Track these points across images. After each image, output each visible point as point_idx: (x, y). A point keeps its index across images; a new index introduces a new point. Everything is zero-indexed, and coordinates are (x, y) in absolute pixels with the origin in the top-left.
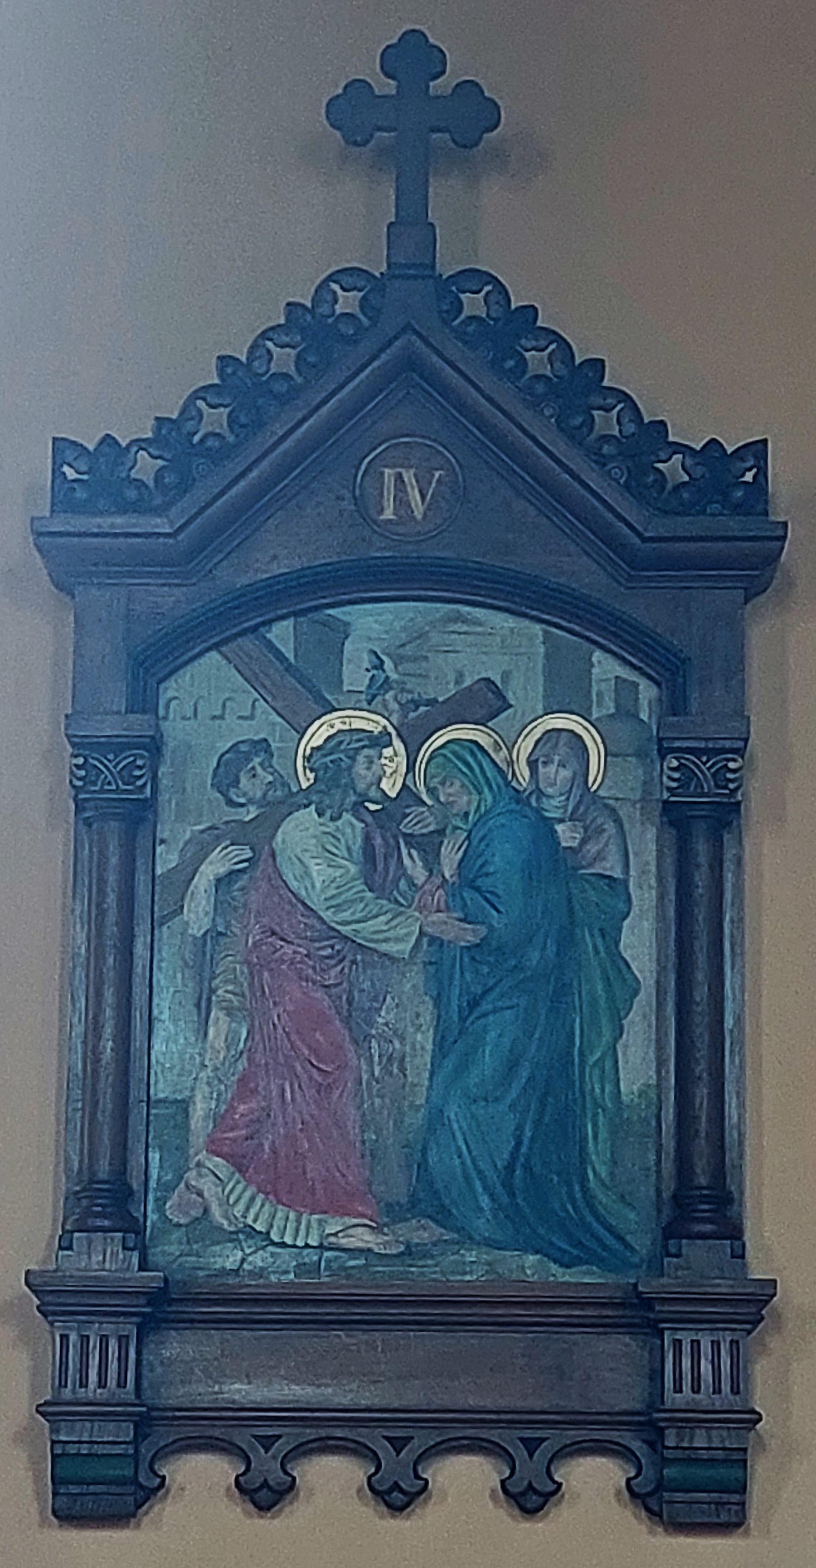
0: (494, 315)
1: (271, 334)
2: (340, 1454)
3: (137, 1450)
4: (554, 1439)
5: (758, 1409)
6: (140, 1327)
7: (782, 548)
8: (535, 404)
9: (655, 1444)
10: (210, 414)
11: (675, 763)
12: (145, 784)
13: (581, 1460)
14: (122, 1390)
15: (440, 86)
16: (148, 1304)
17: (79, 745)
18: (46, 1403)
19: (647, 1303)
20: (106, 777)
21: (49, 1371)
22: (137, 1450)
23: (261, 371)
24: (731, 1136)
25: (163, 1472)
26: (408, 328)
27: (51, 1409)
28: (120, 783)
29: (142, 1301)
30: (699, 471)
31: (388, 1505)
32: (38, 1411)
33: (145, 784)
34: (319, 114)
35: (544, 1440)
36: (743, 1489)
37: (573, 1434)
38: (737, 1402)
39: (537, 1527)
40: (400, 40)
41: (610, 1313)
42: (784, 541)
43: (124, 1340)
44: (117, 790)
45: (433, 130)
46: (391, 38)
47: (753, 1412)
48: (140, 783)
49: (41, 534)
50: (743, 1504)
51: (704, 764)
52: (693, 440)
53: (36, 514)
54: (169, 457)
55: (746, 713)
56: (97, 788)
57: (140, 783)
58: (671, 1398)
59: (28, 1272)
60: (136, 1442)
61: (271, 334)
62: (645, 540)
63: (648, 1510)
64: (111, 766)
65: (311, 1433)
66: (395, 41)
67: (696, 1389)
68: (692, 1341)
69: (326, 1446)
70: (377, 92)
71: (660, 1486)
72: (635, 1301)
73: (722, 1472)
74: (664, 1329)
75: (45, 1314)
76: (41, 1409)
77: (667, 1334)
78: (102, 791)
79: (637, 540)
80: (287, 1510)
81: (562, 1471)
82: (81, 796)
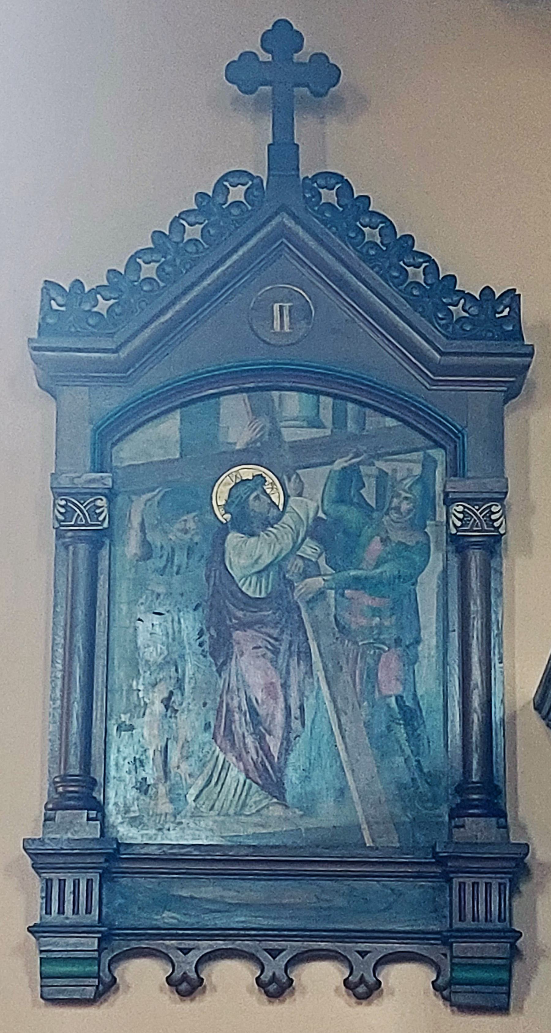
0: (430, 282)
1: (183, 216)
4: (206, 946)
5: (517, 929)
7: (530, 363)
11: (460, 508)
12: (104, 519)
13: (313, 963)
14: (62, 916)
16: (106, 861)
17: (57, 494)
18: (35, 925)
19: (440, 861)
20: (79, 515)
21: (38, 902)
22: (100, 955)
23: (179, 240)
24: (497, 750)
25: (292, 976)
26: (283, 208)
27: (35, 929)
28: (89, 520)
30: (474, 310)
31: (267, 993)
32: (29, 931)
33: (104, 519)
35: (369, 952)
39: (187, 1006)
40: (273, 26)
42: (532, 358)
43: (62, 882)
44: (87, 524)
45: (298, 85)
48: (101, 518)
49: (35, 349)
52: (527, 338)
53: (32, 337)
54: (116, 296)
56: (72, 523)
57: (101, 518)
60: (100, 950)
61: (183, 216)
64: (478, 513)
65: (299, 945)
70: (261, 59)
71: (452, 982)
74: (452, 878)
77: (454, 880)
79: (113, 356)
80: (111, 999)
81: (295, 972)
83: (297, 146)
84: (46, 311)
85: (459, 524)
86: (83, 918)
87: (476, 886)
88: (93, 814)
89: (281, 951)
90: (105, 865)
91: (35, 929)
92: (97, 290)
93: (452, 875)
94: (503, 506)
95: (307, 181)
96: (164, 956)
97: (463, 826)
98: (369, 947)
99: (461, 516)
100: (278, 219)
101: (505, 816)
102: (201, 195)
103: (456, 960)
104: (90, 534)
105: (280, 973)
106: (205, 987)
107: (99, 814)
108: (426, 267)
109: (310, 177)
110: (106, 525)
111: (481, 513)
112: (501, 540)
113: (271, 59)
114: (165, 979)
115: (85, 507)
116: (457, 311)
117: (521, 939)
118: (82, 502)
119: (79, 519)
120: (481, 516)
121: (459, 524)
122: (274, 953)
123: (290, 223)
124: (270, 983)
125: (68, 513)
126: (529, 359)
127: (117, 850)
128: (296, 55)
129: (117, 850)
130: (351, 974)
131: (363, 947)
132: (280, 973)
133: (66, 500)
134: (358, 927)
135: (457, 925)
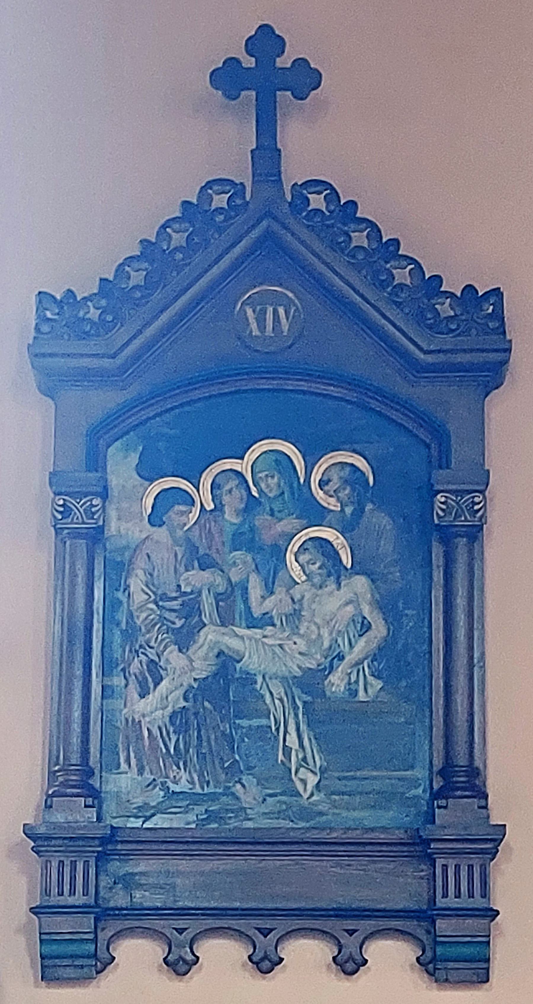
2: (152, 937)
3: (96, 937)
6: (97, 860)
8: (357, 267)
9: (431, 932)
10: (405, 272)
11: (443, 500)
15: (249, 62)
19: (427, 842)
20: (457, 510)
27: (37, 910)
29: (97, 842)
34: (205, 81)
36: (488, 960)
37: (212, 923)
38: (478, 902)
41: (395, 849)
44: (84, 523)
46: (279, 29)
47: (492, 910)
50: (488, 969)
51: (78, 503)
55: (487, 467)
58: (441, 902)
59: (24, 825)
62: (114, 356)
63: (427, 971)
64: (78, 506)
66: (253, 33)
67: (471, 895)
68: (60, 861)
69: (131, 932)
71: (434, 960)
72: (418, 841)
73: (55, 949)
75: (37, 852)
76: (495, 913)
78: (72, 523)
82: (59, 526)
83: (279, 151)
84: (42, 319)
85: (441, 513)
86: (78, 899)
87: (457, 867)
88: (90, 801)
89: (271, 930)
90: (100, 849)
91: (37, 910)
92: (452, 295)
93: (435, 856)
94: (485, 497)
95: (298, 188)
96: (240, 934)
97: (445, 807)
98: (187, 923)
99: (444, 507)
100: (265, 223)
101: (486, 797)
102: (186, 204)
103: (439, 939)
104: (86, 531)
105: (355, 951)
106: (202, 964)
107: (96, 802)
108: (412, 269)
109: (299, 184)
110: (101, 523)
111: (81, 507)
112: (482, 529)
113: (253, 65)
114: (331, 959)
115: (81, 507)
116: (94, 314)
117: (499, 917)
118: (78, 501)
119: (75, 518)
120: (82, 510)
121: (441, 513)
122: (265, 932)
123: (276, 227)
124: (262, 959)
125: (66, 511)
126: (507, 354)
127: (113, 835)
128: (278, 60)
129: (113, 835)
130: (340, 952)
131: (181, 924)
132: (355, 951)
133: (446, 497)
134: (295, 906)
135: (441, 902)
